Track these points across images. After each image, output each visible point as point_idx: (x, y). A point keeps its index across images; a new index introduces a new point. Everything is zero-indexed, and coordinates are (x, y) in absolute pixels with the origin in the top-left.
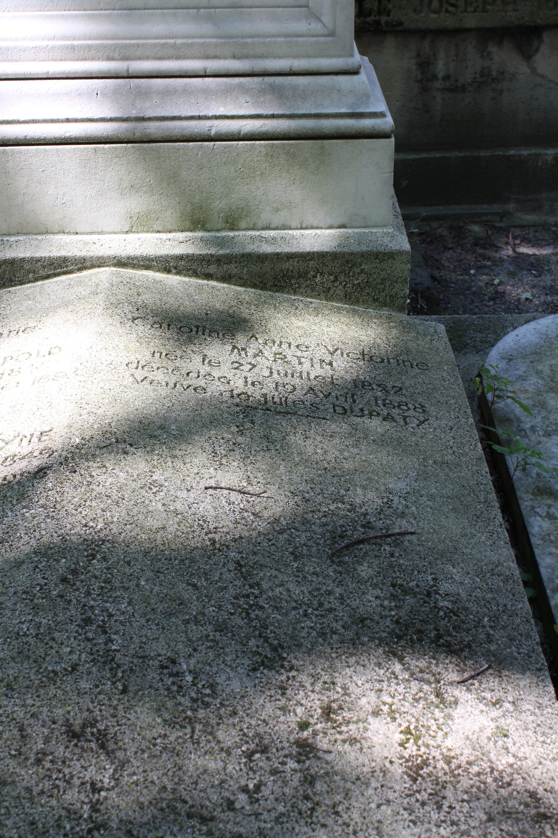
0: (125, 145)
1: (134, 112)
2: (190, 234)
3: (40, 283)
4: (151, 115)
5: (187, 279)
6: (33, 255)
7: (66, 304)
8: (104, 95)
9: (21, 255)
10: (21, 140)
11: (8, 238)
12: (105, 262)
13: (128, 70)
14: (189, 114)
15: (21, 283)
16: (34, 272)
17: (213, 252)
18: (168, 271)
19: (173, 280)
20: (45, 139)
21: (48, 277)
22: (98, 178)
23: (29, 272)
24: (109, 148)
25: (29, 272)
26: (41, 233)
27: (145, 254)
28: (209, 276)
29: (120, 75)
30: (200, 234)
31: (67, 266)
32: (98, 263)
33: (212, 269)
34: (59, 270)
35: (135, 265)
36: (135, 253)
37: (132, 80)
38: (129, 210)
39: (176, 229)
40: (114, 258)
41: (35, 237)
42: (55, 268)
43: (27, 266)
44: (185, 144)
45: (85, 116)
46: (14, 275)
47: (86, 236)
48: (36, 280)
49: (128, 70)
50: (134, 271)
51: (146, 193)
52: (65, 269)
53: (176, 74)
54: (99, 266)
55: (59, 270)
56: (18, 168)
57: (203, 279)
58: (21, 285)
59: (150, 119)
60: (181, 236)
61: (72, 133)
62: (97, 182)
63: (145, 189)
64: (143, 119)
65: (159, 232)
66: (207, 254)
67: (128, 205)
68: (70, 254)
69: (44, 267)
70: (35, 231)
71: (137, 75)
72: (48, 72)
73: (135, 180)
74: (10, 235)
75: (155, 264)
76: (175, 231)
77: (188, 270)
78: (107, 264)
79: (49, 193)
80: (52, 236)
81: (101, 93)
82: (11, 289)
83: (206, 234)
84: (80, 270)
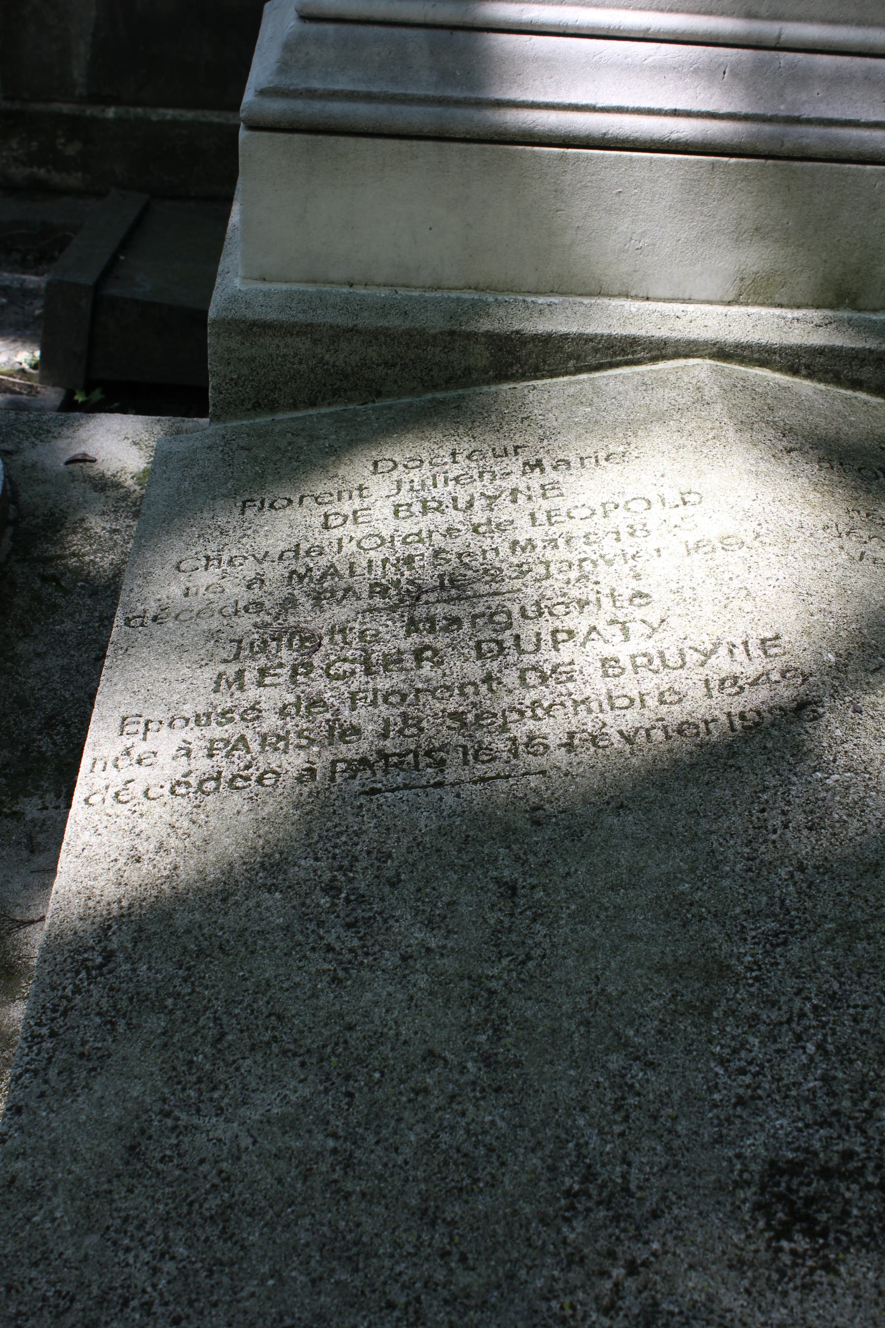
0: (762, 161)
1: (782, 107)
2: (829, 313)
3: (584, 376)
4: (812, 116)
5: (822, 386)
6: (582, 330)
7: (661, 418)
8: (735, 75)
9: (563, 329)
10: (594, 139)
11: (534, 299)
12: (697, 350)
13: (779, 37)
14: (873, 118)
15: (553, 374)
16: (578, 358)
17: (874, 347)
18: (794, 371)
19: (805, 386)
20: (635, 140)
21: (599, 367)
22: (705, 210)
23: (570, 357)
24: (736, 164)
25: (570, 357)
26: (590, 295)
27: (763, 341)
28: (856, 384)
29: (763, 44)
30: (845, 314)
31: (634, 353)
32: (687, 350)
33: (866, 373)
34: (619, 358)
35: (744, 357)
36: (748, 338)
37: (782, 54)
38: (743, 267)
39: (810, 303)
40: (714, 344)
41: (579, 299)
42: (615, 354)
43: (568, 348)
44: (860, 167)
45: (704, 108)
46: (544, 362)
47: (660, 304)
48: (578, 371)
49: (779, 37)
50: (742, 369)
51: (776, 241)
52: (630, 357)
53: (853, 50)
54: (686, 356)
55: (619, 358)
56: (579, 185)
57: (847, 388)
58: (551, 377)
59: (809, 122)
60: (815, 315)
61: (681, 135)
62: (702, 218)
63: (776, 235)
64: (797, 121)
65: (781, 306)
66: (864, 349)
67: (743, 259)
68: (642, 333)
69: (596, 350)
70: (580, 291)
71: (791, 46)
72: (649, 29)
73: (765, 219)
74: (538, 293)
75: (778, 358)
76: (806, 306)
77: (827, 372)
78: (700, 353)
79: (619, 229)
80: (606, 301)
81: (731, 71)
82: (534, 383)
83: (856, 315)
84: (654, 359)
